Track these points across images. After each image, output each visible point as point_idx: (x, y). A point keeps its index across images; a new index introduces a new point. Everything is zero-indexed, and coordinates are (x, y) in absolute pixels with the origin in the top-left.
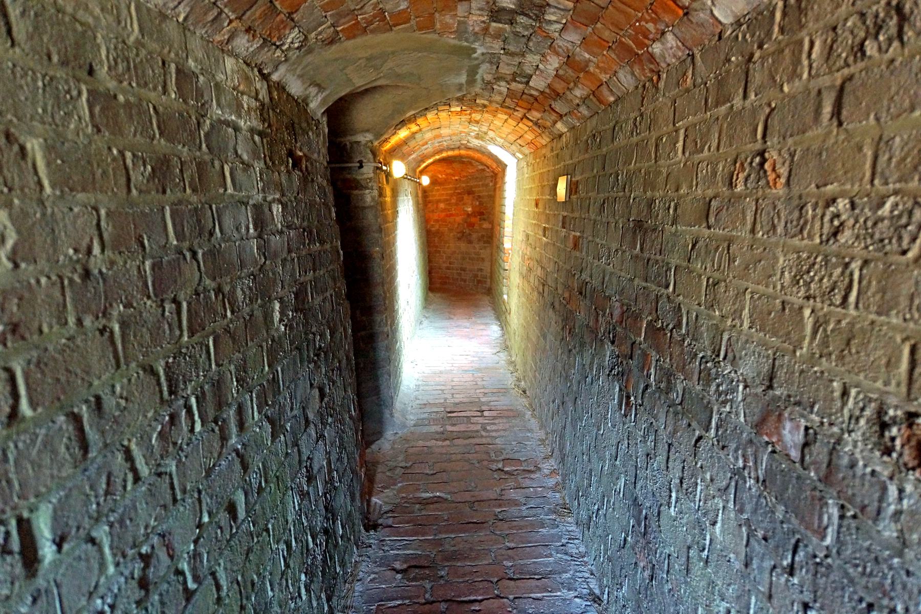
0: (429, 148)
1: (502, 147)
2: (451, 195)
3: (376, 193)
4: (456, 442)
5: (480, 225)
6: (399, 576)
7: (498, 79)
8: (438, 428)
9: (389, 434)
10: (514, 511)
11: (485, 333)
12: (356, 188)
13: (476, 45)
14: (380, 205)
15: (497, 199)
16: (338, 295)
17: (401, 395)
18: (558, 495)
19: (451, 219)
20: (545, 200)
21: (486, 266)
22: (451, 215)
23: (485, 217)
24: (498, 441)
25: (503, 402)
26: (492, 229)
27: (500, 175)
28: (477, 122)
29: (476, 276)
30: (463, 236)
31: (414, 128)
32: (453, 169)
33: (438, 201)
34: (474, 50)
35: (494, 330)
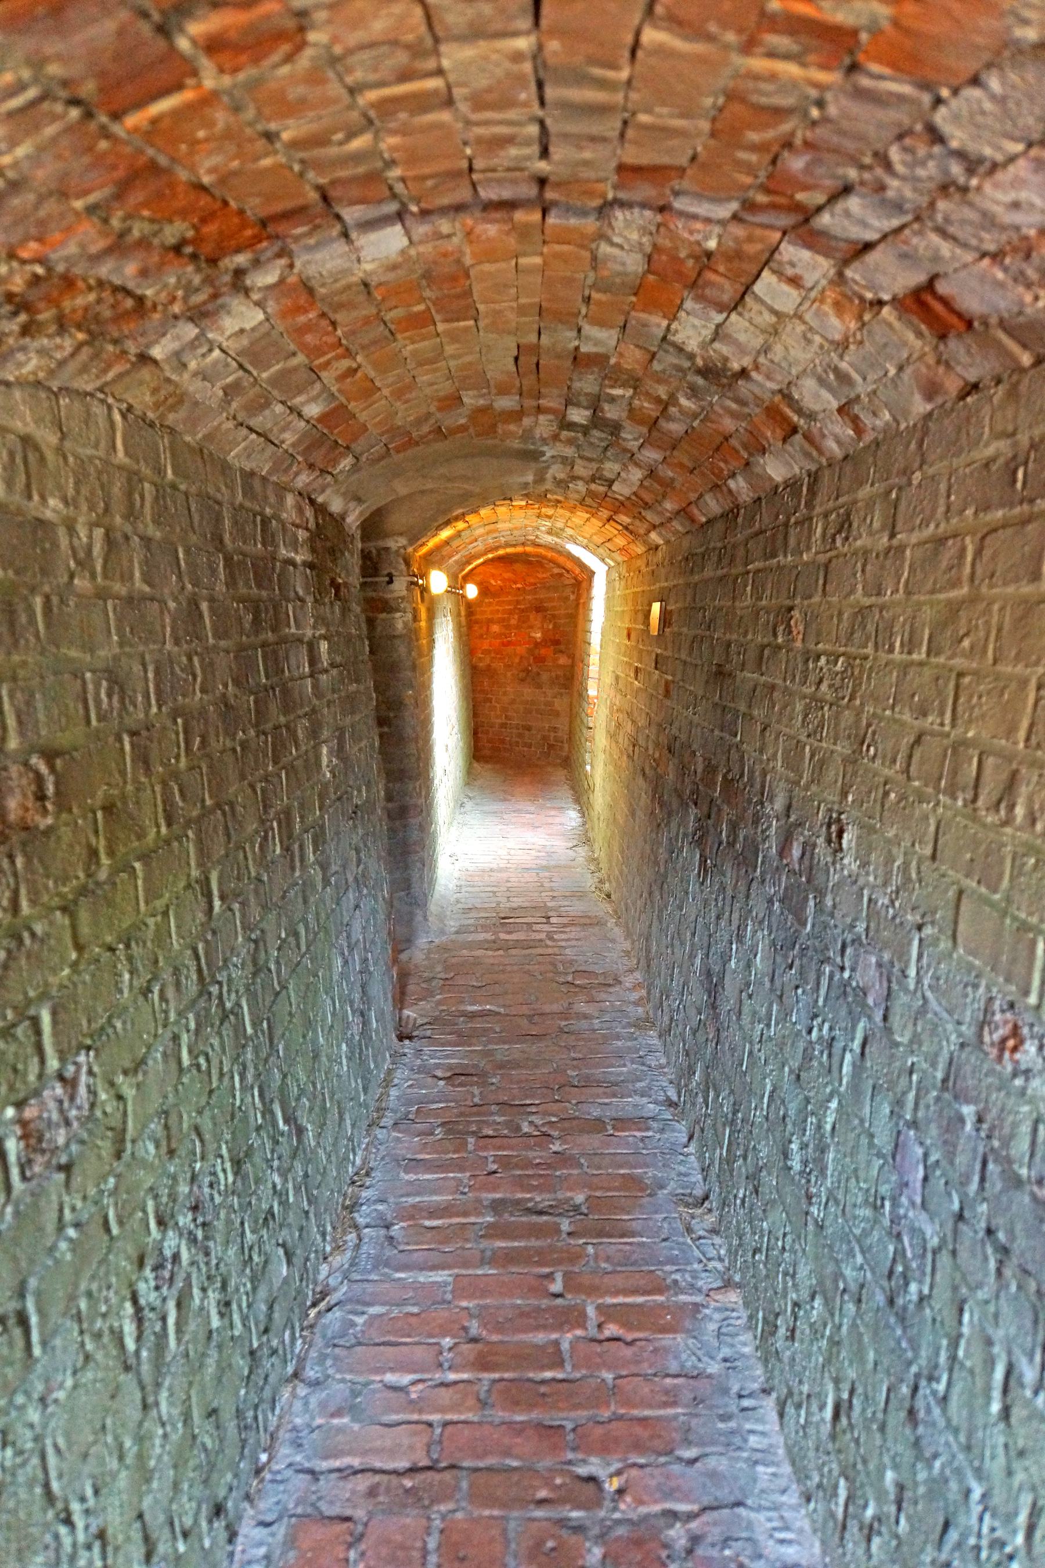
0: (480, 546)
1: (586, 547)
2: (511, 613)
3: (410, 616)
4: (513, 952)
5: (555, 660)
6: (442, 1083)
7: (575, 478)
8: (489, 936)
9: (422, 941)
10: (584, 1024)
11: (557, 820)
12: (383, 610)
13: (545, 448)
14: (412, 635)
15: (580, 621)
16: (372, 746)
17: (436, 895)
18: (640, 1010)
19: (510, 649)
20: (637, 633)
21: (562, 723)
22: (509, 643)
23: (562, 647)
24: (568, 951)
25: (577, 908)
26: (573, 666)
27: (584, 585)
28: (549, 517)
29: (545, 738)
30: (528, 676)
31: (461, 525)
32: (514, 572)
33: (490, 621)
34: (543, 454)
35: (572, 817)
